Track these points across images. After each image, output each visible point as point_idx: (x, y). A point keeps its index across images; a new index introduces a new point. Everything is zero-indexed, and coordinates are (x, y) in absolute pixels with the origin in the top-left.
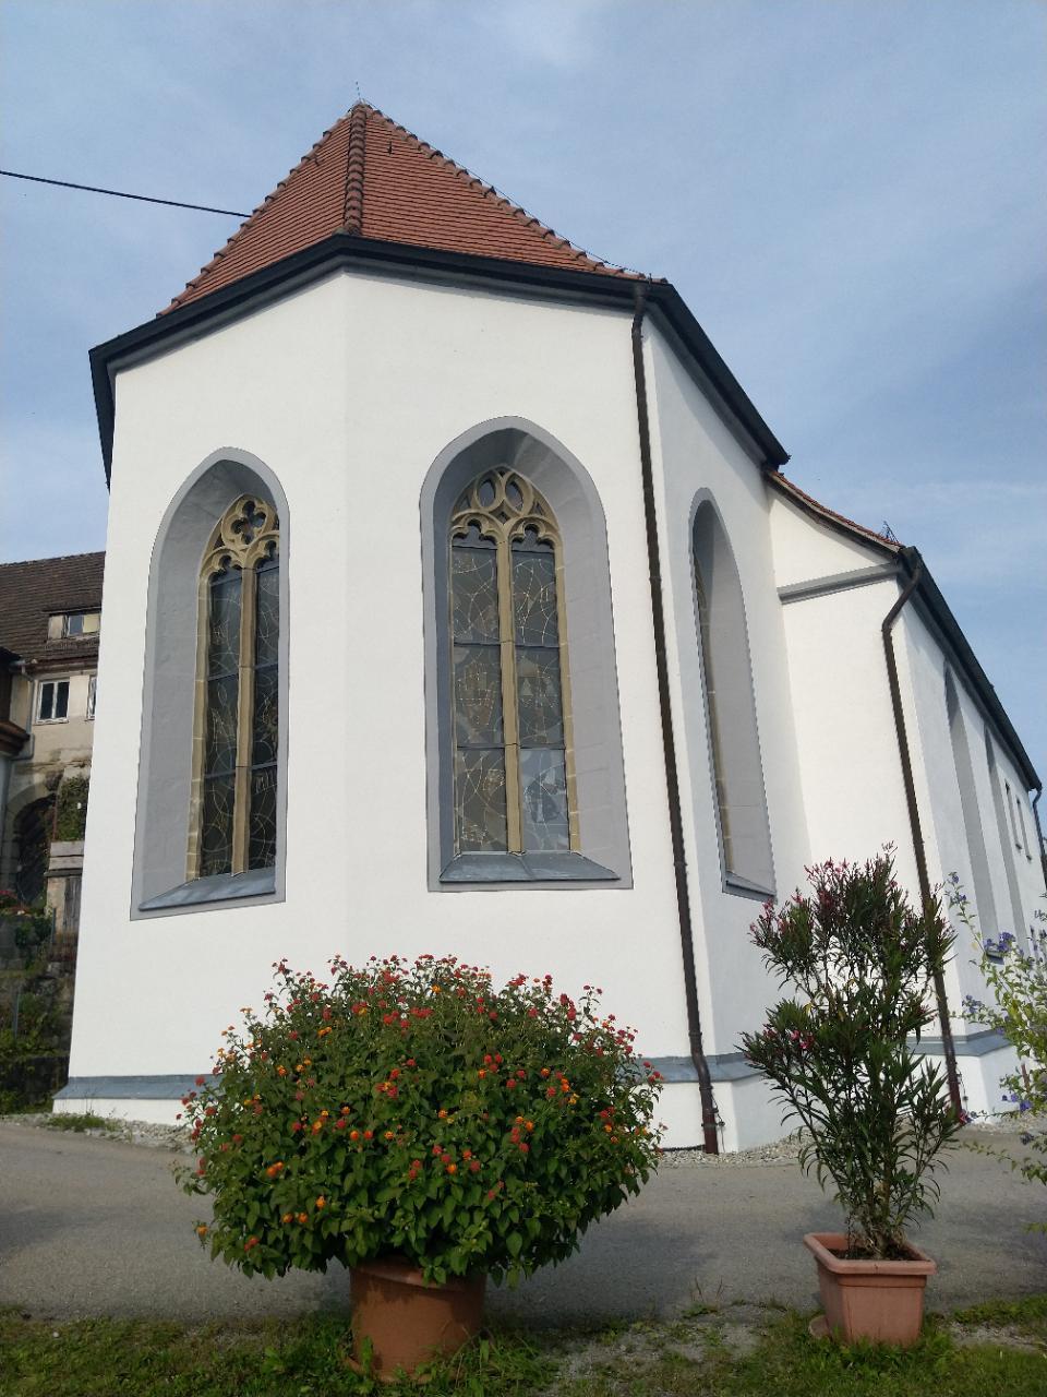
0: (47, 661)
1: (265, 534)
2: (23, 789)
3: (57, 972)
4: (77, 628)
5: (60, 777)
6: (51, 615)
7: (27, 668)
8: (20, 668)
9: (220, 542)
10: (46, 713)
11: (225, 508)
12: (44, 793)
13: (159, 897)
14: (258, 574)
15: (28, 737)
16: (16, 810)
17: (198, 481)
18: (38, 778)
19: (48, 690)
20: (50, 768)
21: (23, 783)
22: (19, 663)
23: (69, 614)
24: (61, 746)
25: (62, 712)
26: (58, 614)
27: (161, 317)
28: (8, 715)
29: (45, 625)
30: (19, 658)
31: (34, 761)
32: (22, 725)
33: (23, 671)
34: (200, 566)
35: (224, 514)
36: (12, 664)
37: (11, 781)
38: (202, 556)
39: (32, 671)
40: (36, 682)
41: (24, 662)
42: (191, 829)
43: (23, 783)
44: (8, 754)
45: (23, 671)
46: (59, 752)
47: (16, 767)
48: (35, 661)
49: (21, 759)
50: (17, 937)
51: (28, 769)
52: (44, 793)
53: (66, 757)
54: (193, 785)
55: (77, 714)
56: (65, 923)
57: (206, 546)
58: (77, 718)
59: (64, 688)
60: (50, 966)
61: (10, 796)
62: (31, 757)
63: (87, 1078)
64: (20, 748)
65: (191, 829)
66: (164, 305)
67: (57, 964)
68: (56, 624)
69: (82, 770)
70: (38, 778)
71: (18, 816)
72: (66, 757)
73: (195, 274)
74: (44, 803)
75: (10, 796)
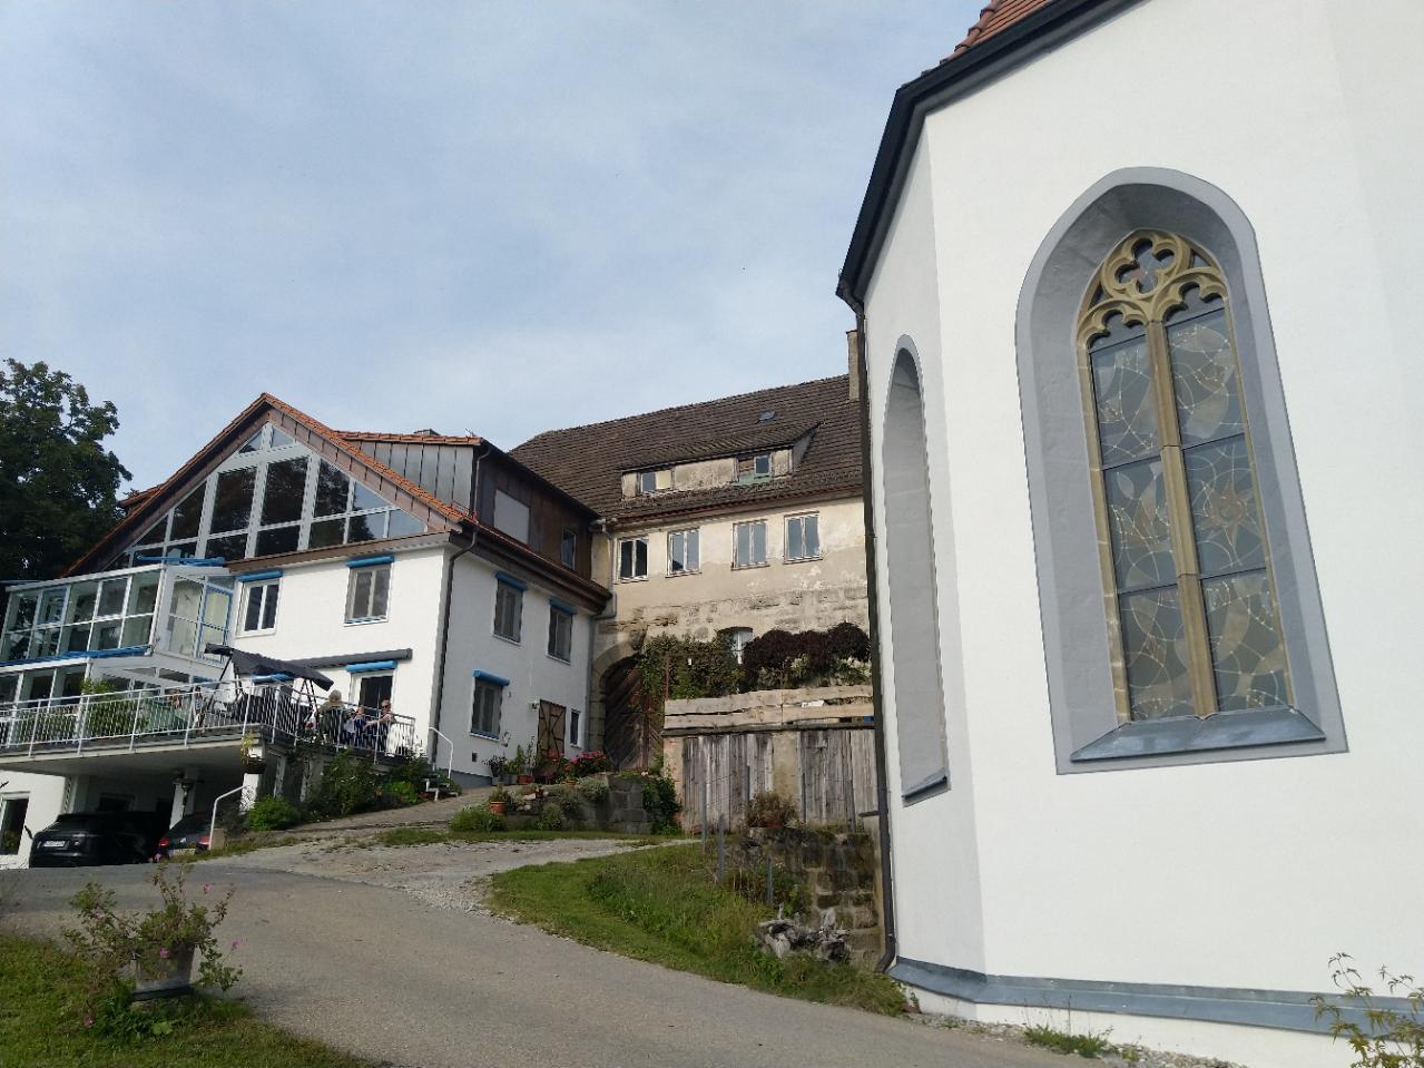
0: (627, 518)
1: (1181, 274)
2: (606, 649)
3: (761, 839)
4: (651, 484)
5: (644, 636)
6: (624, 474)
7: (608, 526)
8: (600, 527)
9: (1099, 292)
10: (625, 572)
11: (1108, 251)
12: (628, 653)
13: (1095, 744)
14: (1167, 328)
15: (611, 596)
16: (602, 670)
17: (1078, 220)
18: (622, 637)
19: (626, 548)
20: (633, 627)
21: (608, 642)
22: (599, 521)
23: (641, 471)
24: (642, 605)
25: (642, 570)
26: (631, 472)
27: (945, 64)
28: (590, 575)
29: (619, 482)
30: (599, 517)
31: (617, 619)
32: (605, 585)
33: (604, 530)
34: (1075, 328)
35: (1105, 260)
36: (593, 523)
37: (596, 641)
38: (1077, 316)
39: (612, 529)
40: (615, 540)
41: (604, 520)
42: (1113, 659)
43: (608, 642)
44: (592, 613)
45: (604, 530)
46: (639, 610)
47: (600, 626)
48: (615, 519)
49: (604, 618)
50: (645, 800)
51: (612, 628)
52: (629, 653)
53: (649, 616)
54: (1106, 600)
55: (656, 572)
56: (685, 786)
57: (1081, 303)
58: (659, 575)
59: (642, 549)
60: (752, 832)
61: (596, 657)
62: (614, 616)
63: (1144, 988)
64: (603, 607)
65: (1113, 659)
66: (949, 52)
67: (760, 830)
68: (630, 482)
69: (665, 629)
70: (622, 637)
71: (603, 676)
72: (649, 616)
73: (975, 20)
74: (629, 662)
75: (596, 657)
